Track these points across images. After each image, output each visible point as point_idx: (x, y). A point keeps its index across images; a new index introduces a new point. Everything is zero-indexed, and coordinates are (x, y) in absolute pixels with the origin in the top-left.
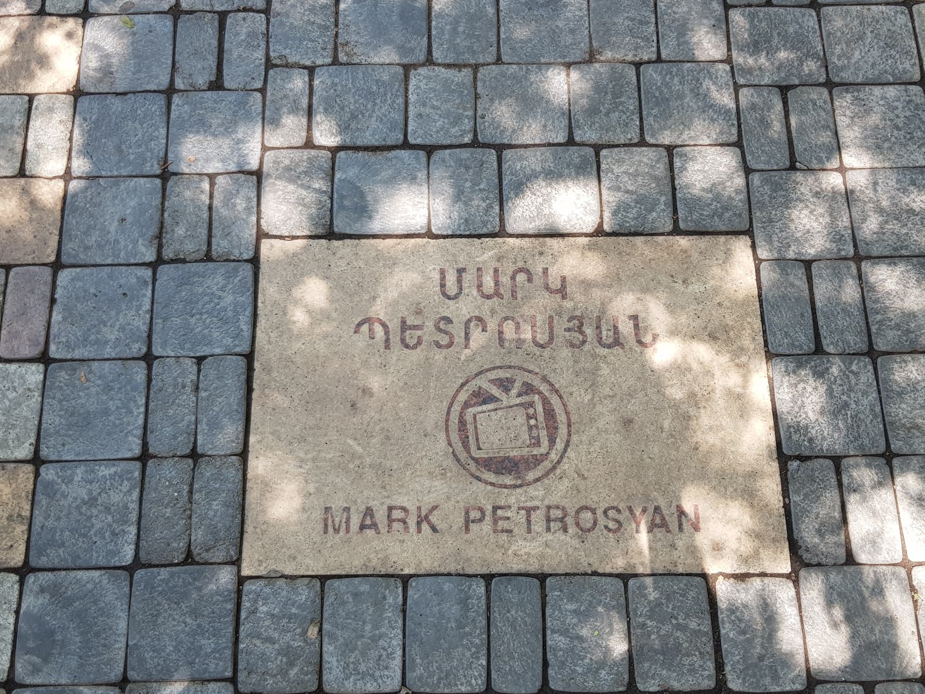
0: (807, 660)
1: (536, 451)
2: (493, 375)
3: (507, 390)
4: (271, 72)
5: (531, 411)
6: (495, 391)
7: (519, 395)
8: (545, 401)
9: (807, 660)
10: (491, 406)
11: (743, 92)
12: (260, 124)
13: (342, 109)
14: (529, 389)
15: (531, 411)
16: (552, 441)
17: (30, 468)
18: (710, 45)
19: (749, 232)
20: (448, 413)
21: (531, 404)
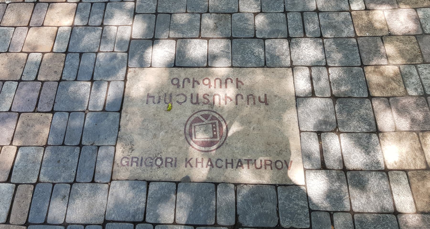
0: (340, 140)
1: (215, 140)
2: (203, 113)
3: (206, 119)
4: (18, 113)
5: (214, 125)
6: (203, 119)
7: (201, 115)
8: (219, 121)
9: (340, 140)
10: (201, 123)
11: (116, 28)
12: (213, 69)
13: (250, 58)
14: (213, 118)
15: (214, 125)
16: (221, 137)
17: (78, 148)
18: (377, 61)
19: (297, 97)
20: (201, 111)
21: (215, 123)
